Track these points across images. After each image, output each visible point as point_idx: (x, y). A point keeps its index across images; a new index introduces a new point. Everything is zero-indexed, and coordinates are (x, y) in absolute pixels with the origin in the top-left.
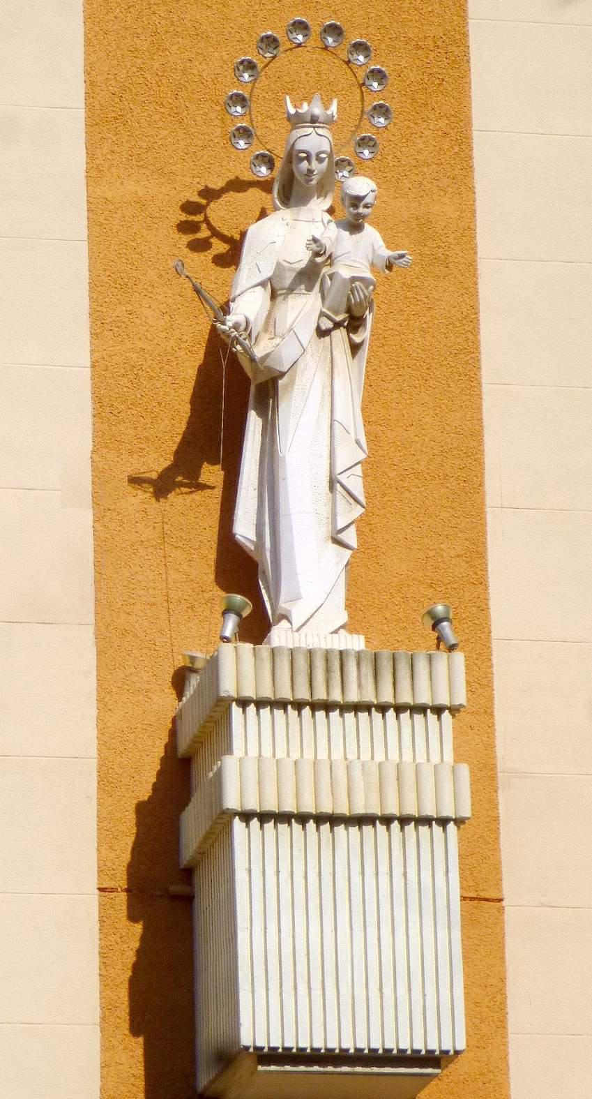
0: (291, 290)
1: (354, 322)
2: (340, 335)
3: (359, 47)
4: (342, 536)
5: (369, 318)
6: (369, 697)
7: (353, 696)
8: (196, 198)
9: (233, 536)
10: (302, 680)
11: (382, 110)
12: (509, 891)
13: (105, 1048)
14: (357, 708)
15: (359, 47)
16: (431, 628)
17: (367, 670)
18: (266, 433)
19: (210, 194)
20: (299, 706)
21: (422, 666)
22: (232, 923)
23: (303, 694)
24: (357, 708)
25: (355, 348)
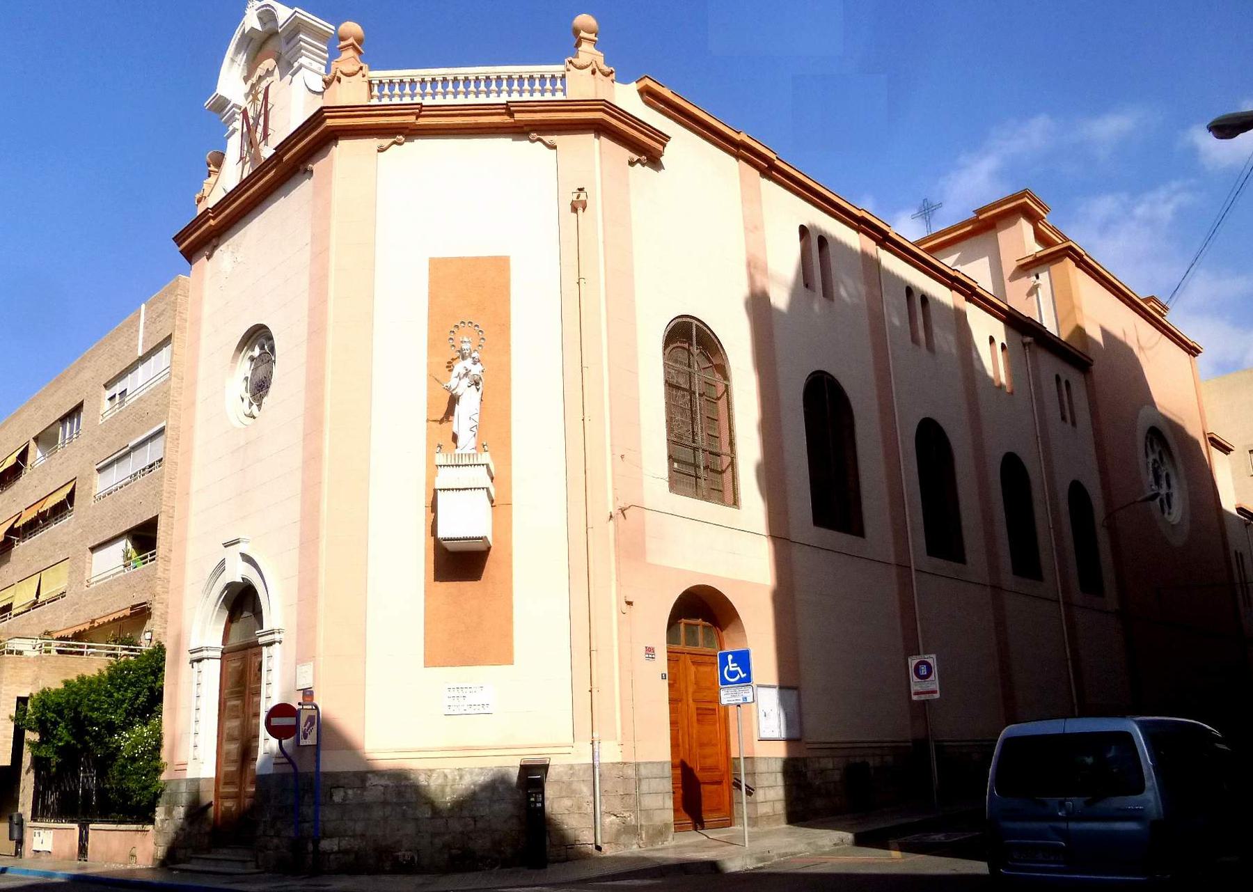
0: (463, 378)
1: (477, 384)
2: (474, 387)
3: (476, 326)
4: (472, 429)
5: (481, 383)
6: (467, 463)
7: (464, 463)
8: (450, 360)
9: (1033, 225)
10: (453, 461)
11: (483, 339)
12: (513, 503)
13: (426, 539)
14: (466, 465)
15: (476, 326)
16: (1070, 383)
17: (467, 457)
18: (109, 650)
19: (453, 359)
20: (453, 466)
21: (479, 455)
22: (182, 239)
23: (453, 463)
24: (466, 465)
25: (478, 390)
